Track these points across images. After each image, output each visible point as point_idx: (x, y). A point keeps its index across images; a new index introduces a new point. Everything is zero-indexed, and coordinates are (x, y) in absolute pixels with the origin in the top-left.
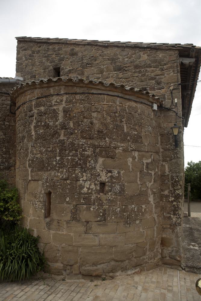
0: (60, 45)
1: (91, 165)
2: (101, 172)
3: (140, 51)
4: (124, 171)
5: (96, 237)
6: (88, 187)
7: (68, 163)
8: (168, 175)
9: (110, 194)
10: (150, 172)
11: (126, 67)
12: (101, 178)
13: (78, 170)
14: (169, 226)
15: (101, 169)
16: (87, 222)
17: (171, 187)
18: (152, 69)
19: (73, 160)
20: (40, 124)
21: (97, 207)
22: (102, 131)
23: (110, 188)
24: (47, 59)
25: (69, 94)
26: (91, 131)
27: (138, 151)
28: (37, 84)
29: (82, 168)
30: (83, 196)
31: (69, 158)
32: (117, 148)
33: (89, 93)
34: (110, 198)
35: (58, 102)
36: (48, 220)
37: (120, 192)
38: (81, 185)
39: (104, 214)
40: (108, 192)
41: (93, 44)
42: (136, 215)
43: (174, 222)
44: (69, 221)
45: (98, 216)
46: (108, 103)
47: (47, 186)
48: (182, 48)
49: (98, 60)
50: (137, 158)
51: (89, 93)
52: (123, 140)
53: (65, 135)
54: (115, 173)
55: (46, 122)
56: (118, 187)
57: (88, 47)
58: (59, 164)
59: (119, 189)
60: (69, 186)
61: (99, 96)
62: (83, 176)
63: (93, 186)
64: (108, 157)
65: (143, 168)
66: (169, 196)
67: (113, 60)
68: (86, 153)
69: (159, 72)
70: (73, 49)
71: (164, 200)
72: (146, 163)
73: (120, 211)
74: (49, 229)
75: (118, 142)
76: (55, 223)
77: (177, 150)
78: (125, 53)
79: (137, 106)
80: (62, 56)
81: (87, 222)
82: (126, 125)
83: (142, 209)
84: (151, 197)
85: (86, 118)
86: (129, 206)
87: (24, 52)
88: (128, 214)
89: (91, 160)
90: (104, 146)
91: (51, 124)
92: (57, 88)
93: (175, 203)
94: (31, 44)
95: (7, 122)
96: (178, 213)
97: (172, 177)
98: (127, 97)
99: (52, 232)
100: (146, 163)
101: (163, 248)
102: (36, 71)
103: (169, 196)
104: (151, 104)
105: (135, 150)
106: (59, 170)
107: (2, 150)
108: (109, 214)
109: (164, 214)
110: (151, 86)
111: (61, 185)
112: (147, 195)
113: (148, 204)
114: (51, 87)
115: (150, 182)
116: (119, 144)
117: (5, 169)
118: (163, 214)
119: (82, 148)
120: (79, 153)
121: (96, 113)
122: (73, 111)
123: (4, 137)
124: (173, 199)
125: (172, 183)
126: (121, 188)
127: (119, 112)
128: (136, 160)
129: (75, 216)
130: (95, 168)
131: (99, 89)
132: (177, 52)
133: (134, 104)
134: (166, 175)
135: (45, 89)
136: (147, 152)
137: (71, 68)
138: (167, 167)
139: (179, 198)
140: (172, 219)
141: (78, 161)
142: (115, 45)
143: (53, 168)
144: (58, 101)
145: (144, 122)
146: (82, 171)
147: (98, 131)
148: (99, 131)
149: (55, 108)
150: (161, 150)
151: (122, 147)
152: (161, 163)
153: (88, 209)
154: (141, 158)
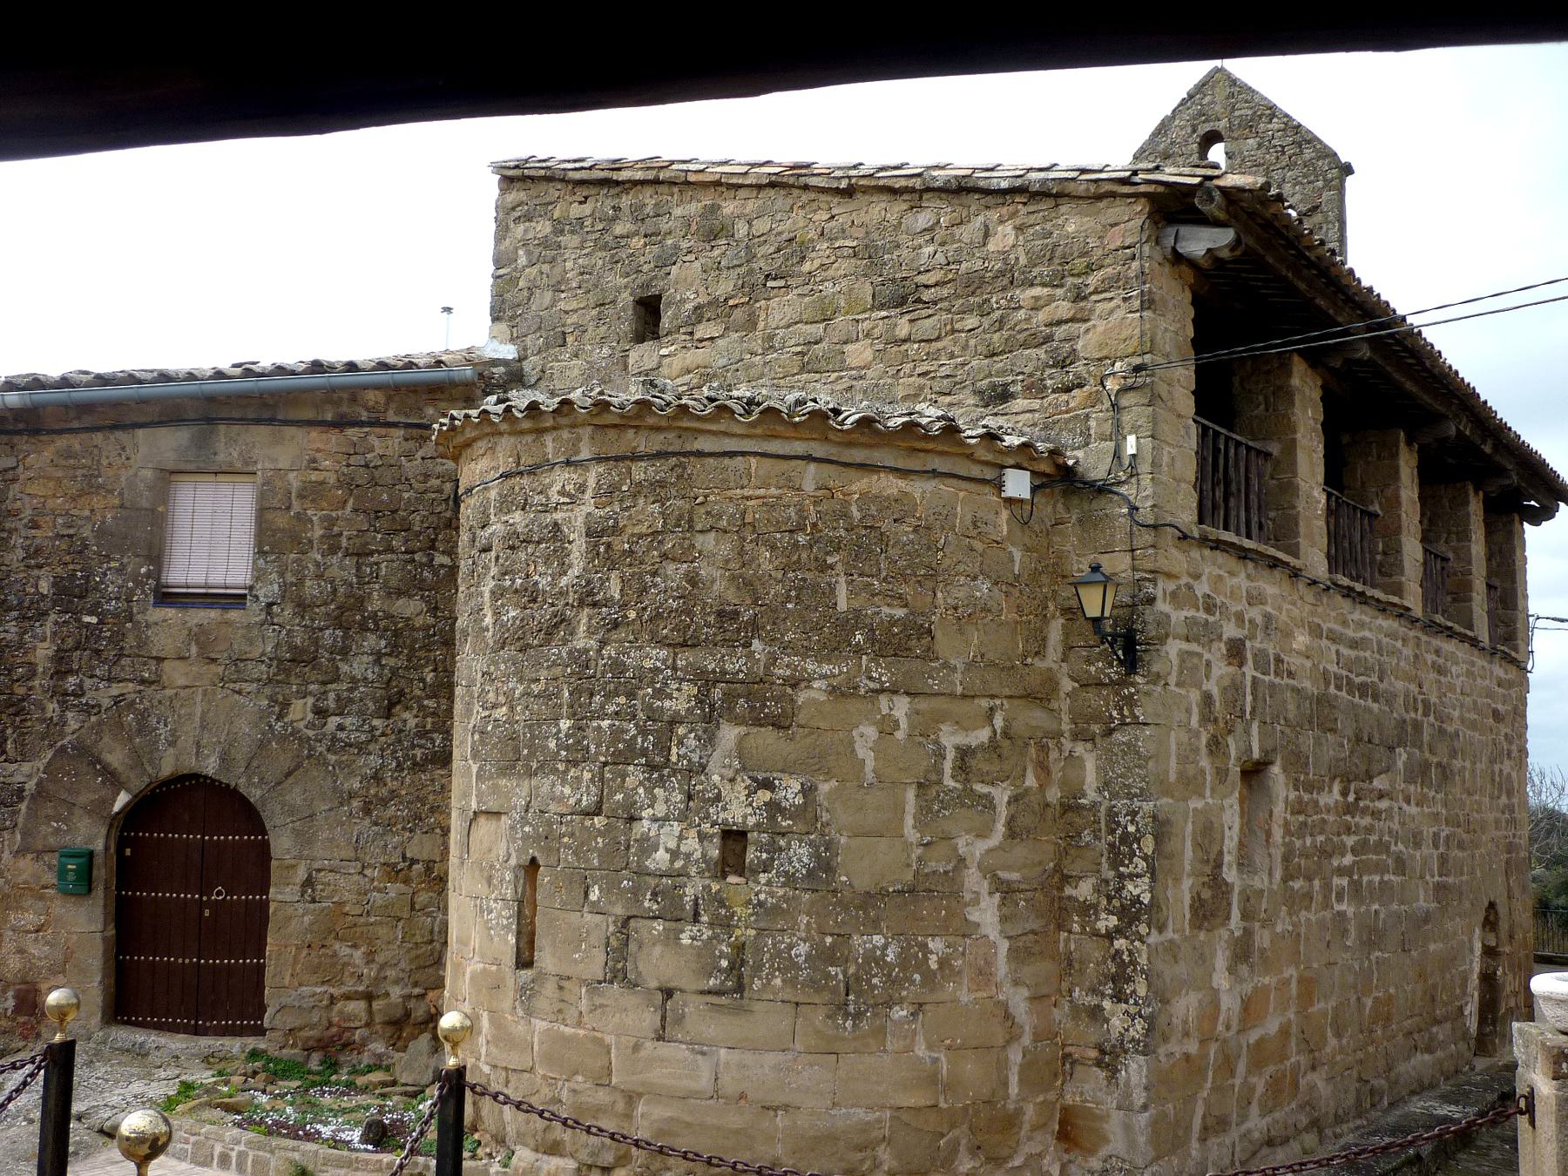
0: (661, 189)
1: (685, 756)
2: (728, 787)
3: (987, 207)
4: (834, 783)
5: (699, 1057)
6: (672, 844)
7: (598, 746)
8: (1094, 805)
9: (763, 878)
10: (980, 788)
11: (927, 287)
12: (724, 809)
13: (635, 775)
14: (1093, 1054)
15: (730, 774)
16: (668, 993)
17: (1105, 866)
18: (1037, 291)
19: (617, 733)
20: (508, 583)
21: (707, 933)
22: (737, 613)
23: (764, 856)
24: (612, 256)
25: (608, 459)
26: (689, 613)
27: (907, 694)
28: (520, 415)
29: (651, 767)
30: (652, 882)
31: (605, 724)
32: (803, 685)
33: (686, 454)
34: (762, 897)
35: (569, 495)
36: (526, 974)
37: (811, 874)
38: (645, 838)
39: (737, 964)
40: (755, 872)
41: (792, 180)
42: (891, 981)
43: (1115, 1035)
44: (600, 982)
45: (710, 970)
46: (762, 492)
47: (526, 837)
48: (1161, 189)
49: (814, 255)
50: (904, 724)
51: (686, 454)
52: (830, 651)
53: (590, 632)
54: (790, 791)
55: (528, 576)
56: (800, 854)
57: (772, 192)
58: (567, 748)
59: (805, 860)
60: (600, 840)
61: (727, 461)
62: (654, 799)
63: (692, 844)
64: (758, 723)
65: (940, 772)
66: (1095, 907)
67: (869, 255)
68: (667, 704)
69: (1064, 309)
70: (714, 208)
71: (1076, 927)
72: (957, 748)
73: (809, 957)
74: (530, 1013)
75: (804, 657)
76: (550, 988)
77: (1133, 684)
78: (923, 219)
79: (908, 489)
80: (670, 242)
81: (668, 993)
82: (850, 583)
83: (925, 955)
84: (983, 905)
85: (674, 560)
86: (856, 940)
87: (521, 227)
88: (852, 970)
89: (685, 736)
90: (741, 676)
91: (543, 583)
92: (565, 434)
93: (1122, 941)
94: (553, 191)
95: (443, 553)
96: (1134, 992)
97: (1112, 815)
98: (858, 455)
99: (540, 1025)
100: (957, 748)
101: (1066, 1157)
102: (566, 312)
103: (1095, 907)
104: (989, 474)
105: (895, 692)
106: (566, 772)
107: (422, 680)
108: (758, 968)
109: (1076, 994)
110: (1031, 375)
111: (572, 835)
112: (956, 894)
113: (964, 936)
114: (545, 430)
115: (982, 835)
116: (810, 666)
117: (433, 762)
118: (1070, 992)
119: (652, 683)
120: (639, 707)
121: (713, 534)
122: (622, 531)
123: (431, 621)
124: (1113, 921)
125: (1112, 845)
126: (816, 856)
127: (814, 525)
128: (900, 735)
129: (620, 966)
130: (703, 767)
131: (725, 434)
132: (1140, 206)
133: (890, 485)
134: (1083, 807)
135: (529, 438)
136: (964, 696)
137: (703, 299)
138: (1090, 766)
139: (1136, 918)
140: (1107, 1021)
141: (634, 737)
142: (881, 183)
143: (547, 767)
144: (570, 488)
145: (947, 562)
146: (649, 779)
147: (720, 614)
148: (724, 611)
149: (558, 516)
150: (1067, 685)
151: (824, 677)
152: (1067, 744)
153: (672, 938)
154: (924, 729)
